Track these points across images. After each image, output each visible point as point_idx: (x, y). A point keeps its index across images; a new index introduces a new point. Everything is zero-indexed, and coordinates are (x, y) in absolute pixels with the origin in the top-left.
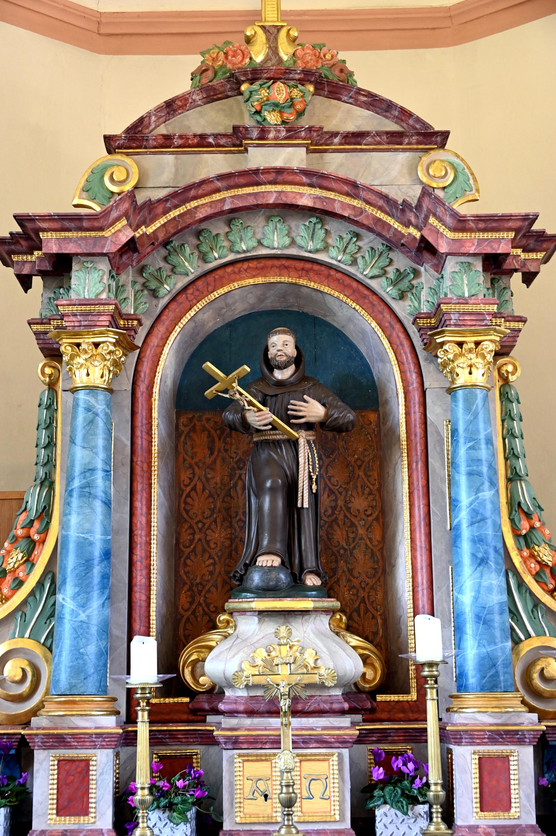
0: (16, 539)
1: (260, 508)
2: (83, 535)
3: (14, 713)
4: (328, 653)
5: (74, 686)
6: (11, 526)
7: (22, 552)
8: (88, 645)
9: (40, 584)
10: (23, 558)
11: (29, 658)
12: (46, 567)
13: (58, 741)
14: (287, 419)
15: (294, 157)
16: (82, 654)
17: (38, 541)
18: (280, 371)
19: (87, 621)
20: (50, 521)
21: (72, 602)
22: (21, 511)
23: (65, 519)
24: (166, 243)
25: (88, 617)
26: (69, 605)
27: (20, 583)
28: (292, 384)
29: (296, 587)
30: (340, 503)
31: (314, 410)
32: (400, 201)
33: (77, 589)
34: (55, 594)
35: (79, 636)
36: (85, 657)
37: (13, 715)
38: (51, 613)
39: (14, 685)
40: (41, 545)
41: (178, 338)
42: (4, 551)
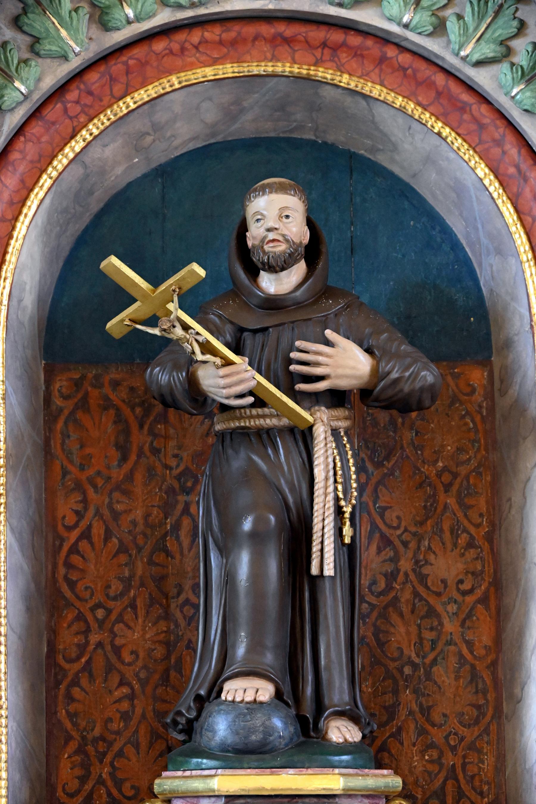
1: (229, 578)
14: (288, 382)
18: (272, 276)
28: (299, 305)
29: (308, 745)
30: (405, 565)
31: (346, 362)
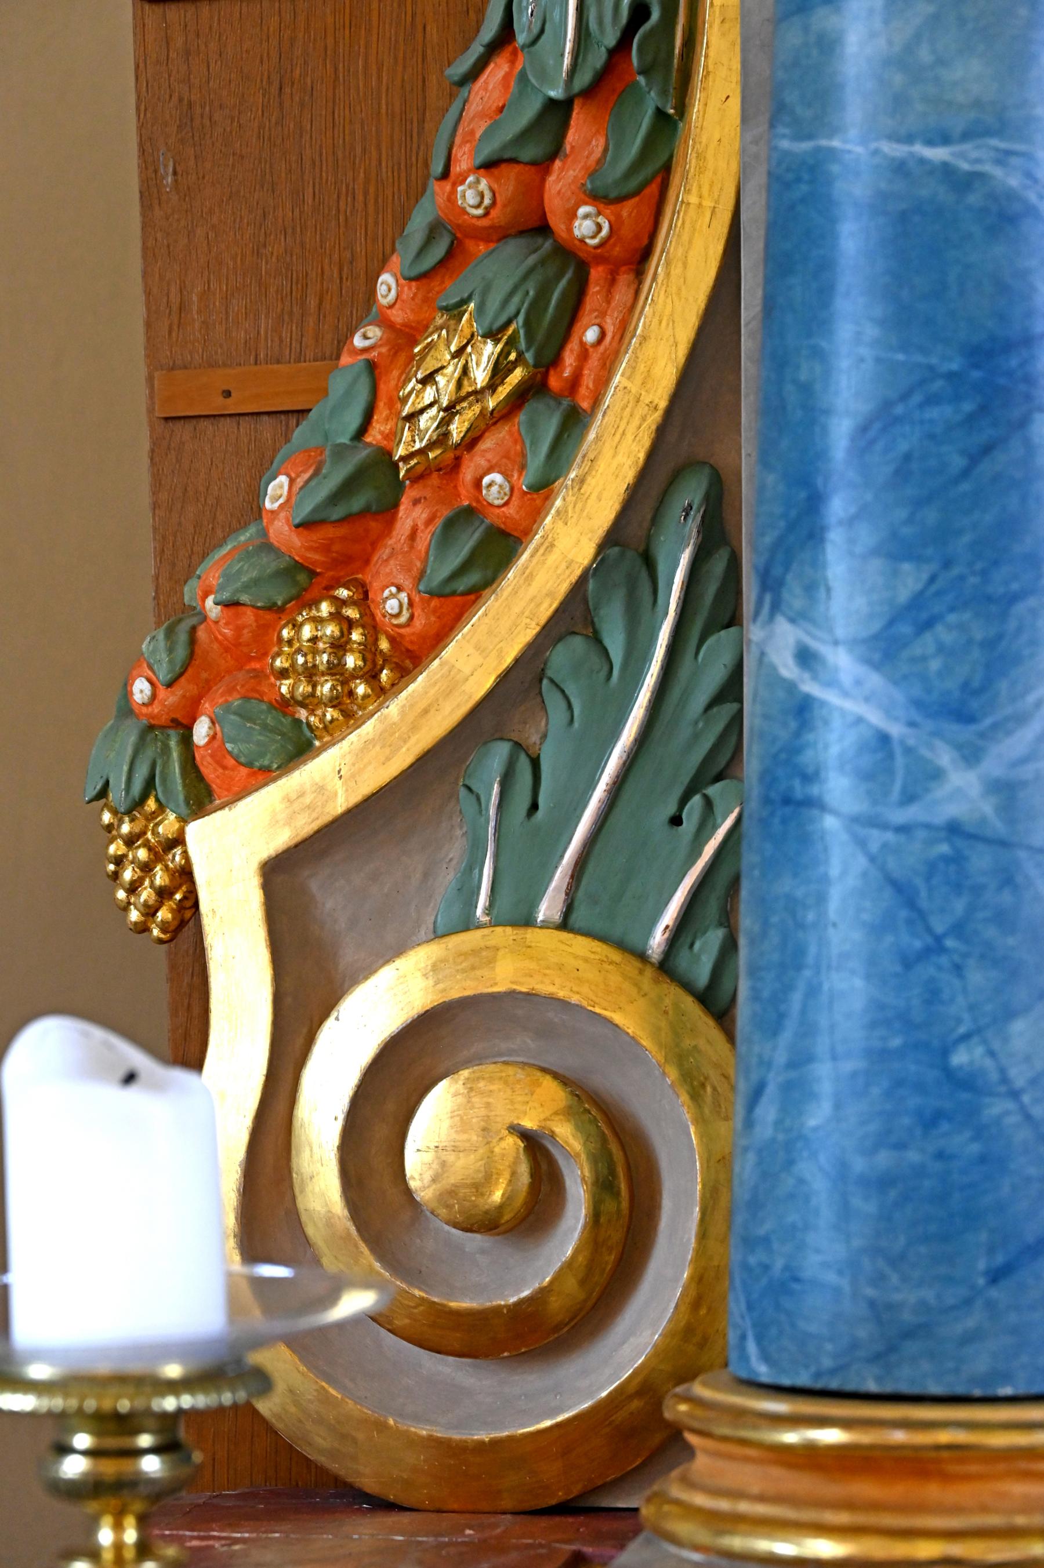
0: (454, 246)
2: (938, 154)
3: (484, 1436)
5: (909, 1334)
6: (418, 170)
7: (493, 335)
8: (1009, 1014)
9: (627, 549)
10: (499, 371)
11: (569, 1061)
12: (661, 431)
16: (965, 1082)
17: (601, 254)
19: (998, 827)
20: (682, 108)
21: (875, 680)
22: (477, 50)
23: (793, 37)
25: (1006, 791)
26: (853, 707)
27: (499, 547)
33: (911, 580)
34: (734, 620)
35: (937, 947)
36: (996, 1108)
37: (481, 1447)
38: (717, 746)
39: (475, 1241)
40: (625, 279)
41: (276, 1528)
42: (375, 332)
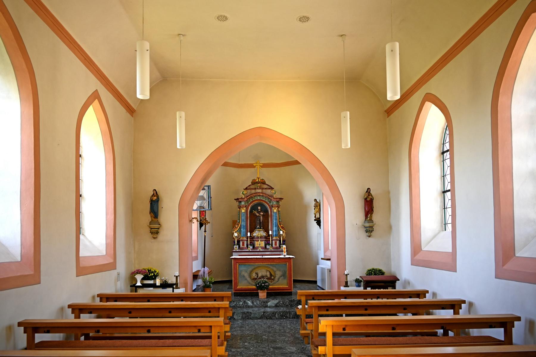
4: (263, 233)
13: (242, 240)
15: (260, 191)
24: (249, 199)
31: (262, 214)
32: (26, 334)
